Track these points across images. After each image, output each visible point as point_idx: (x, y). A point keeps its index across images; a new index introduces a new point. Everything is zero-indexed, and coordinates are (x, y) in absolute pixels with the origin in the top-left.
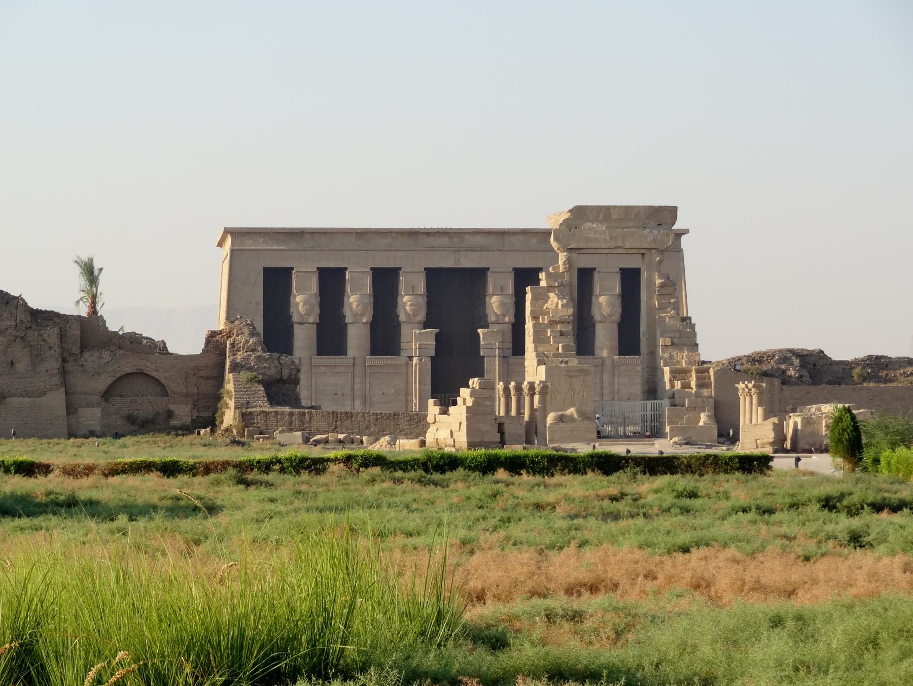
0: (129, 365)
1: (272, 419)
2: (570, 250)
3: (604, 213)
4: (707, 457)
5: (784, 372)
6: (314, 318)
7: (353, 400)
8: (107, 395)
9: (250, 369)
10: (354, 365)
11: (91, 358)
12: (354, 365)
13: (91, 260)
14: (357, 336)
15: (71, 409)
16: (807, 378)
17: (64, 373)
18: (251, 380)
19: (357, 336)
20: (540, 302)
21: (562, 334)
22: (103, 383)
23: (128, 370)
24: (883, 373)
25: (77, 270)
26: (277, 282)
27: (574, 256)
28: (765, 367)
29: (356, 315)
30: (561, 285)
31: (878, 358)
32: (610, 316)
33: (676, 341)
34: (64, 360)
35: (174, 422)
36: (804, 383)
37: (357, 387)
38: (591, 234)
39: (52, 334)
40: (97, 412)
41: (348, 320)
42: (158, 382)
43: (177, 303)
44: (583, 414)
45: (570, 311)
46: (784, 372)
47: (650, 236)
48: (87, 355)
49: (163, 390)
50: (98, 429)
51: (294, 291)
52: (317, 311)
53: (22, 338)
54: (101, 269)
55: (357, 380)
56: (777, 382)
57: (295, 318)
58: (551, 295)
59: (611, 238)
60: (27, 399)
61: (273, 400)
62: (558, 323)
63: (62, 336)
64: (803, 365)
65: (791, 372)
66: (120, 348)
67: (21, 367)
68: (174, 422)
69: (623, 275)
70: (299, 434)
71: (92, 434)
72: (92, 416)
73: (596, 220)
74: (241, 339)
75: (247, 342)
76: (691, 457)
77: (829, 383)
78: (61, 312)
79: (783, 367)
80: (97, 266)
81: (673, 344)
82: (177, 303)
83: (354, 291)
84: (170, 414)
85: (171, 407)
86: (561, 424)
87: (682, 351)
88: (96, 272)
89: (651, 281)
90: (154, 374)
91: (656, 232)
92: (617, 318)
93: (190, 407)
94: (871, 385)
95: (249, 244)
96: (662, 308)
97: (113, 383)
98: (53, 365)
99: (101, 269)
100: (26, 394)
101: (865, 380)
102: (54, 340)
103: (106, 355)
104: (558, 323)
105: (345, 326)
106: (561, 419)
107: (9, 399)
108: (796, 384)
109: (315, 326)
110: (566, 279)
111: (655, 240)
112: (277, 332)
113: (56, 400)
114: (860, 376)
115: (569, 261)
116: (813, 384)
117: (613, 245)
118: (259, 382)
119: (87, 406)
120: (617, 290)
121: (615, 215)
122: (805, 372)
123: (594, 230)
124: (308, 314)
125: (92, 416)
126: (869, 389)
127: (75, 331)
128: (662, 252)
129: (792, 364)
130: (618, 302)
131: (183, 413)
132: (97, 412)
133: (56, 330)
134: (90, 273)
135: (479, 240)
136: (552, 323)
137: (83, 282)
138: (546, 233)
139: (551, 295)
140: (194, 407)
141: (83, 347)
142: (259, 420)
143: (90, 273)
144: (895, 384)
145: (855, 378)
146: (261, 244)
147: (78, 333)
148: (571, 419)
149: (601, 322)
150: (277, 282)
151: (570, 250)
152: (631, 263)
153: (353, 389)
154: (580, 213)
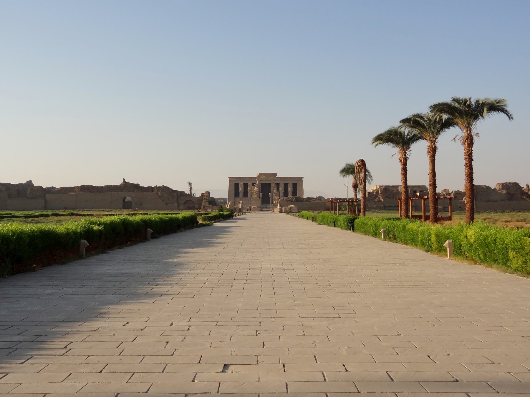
3: (265, 174)
6: (243, 191)
8: (184, 203)
14: (241, 194)
15: (178, 206)
17: (177, 200)
19: (241, 194)
22: (184, 201)
26: (237, 186)
43: (221, 191)
44: (258, 207)
47: (272, 178)
49: (193, 203)
61: (210, 204)
63: (177, 194)
78: (58, 186)
82: (221, 191)
112: (237, 194)
113: (176, 204)
123: (263, 177)
131: (197, 206)
150: (237, 186)
152: (286, 182)
154: (260, 174)
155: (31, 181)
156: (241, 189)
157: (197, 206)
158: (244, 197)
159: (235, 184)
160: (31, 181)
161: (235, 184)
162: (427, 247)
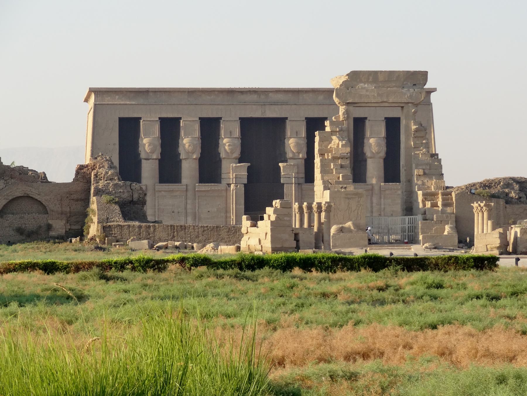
0: (19, 190)
1: (126, 231)
2: (348, 104)
4: (450, 258)
5: (507, 194)
6: (156, 155)
7: (186, 216)
9: (109, 193)
10: (187, 190)
12: (187, 190)
14: (189, 168)
18: (110, 202)
19: (189, 168)
20: (326, 143)
21: (342, 166)
23: (18, 194)
26: (129, 128)
27: (351, 108)
29: (188, 153)
30: (341, 130)
32: (378, 153)
33: (427, 172)
35: (52, 233)
36: (523, 203)
37: (189, 206)
38: (364, 92)
41: (182, 156)
44: (357, 226)
46: (507, 194)
47: (407, 94)
49: (44, 210)
51: (142, 135)
55: (189, 202)
56: (502, 202)
57: (143, 156)
58: (334, 137)
59: (379, 95)
61: (126, 216)
62: (339, 158)
64: (521, 190)
65: (513, 194)
68: (52, 233)
69: (387, 123)
70: (146, 242)
73: (367, 82)
74: (102, 171)
75: (107, 173)
76: (438, 258)
79: (507, 190)
81: (425, 174)
83: (186, 135)
84: (49, 227)
85: (50, 222)
86: (342, 234)
87: (431, 179)
89: (408, 127)
90: (37, 197)
91: (412, 90)
92: (383, 154)
93: (64, 222)
95: (107, 100)
96: (416, 147)
104: (339, 158)
108: (516, 203)
109: (157, 161)
110: (345, 126)
111: (411, 96)
112: (129, 165)
115: (347, 112)
120: (383, 134)
121: (381, 78)
122: (522, 195)
123: (366, 89)
124: (152, 152)
129: (513, 189)
130: (383, 143)
131: (59, 226)
136: (335, 159)
138: (330, 92)
139: (334, 137)
142: (116, 231)
146: (118, 100)
148: (349, 230)
149: (371, 158)
150: (129, 128)
151: (348, 104)
152: (209, 113)
153: (186, 208)
155: (427, 72)
156: (148, 143)
157: (59, 226)
158: (202, 180)
159: (122, 121)
160: (427, 72)
161: (122, 121)
162: (97, 229)
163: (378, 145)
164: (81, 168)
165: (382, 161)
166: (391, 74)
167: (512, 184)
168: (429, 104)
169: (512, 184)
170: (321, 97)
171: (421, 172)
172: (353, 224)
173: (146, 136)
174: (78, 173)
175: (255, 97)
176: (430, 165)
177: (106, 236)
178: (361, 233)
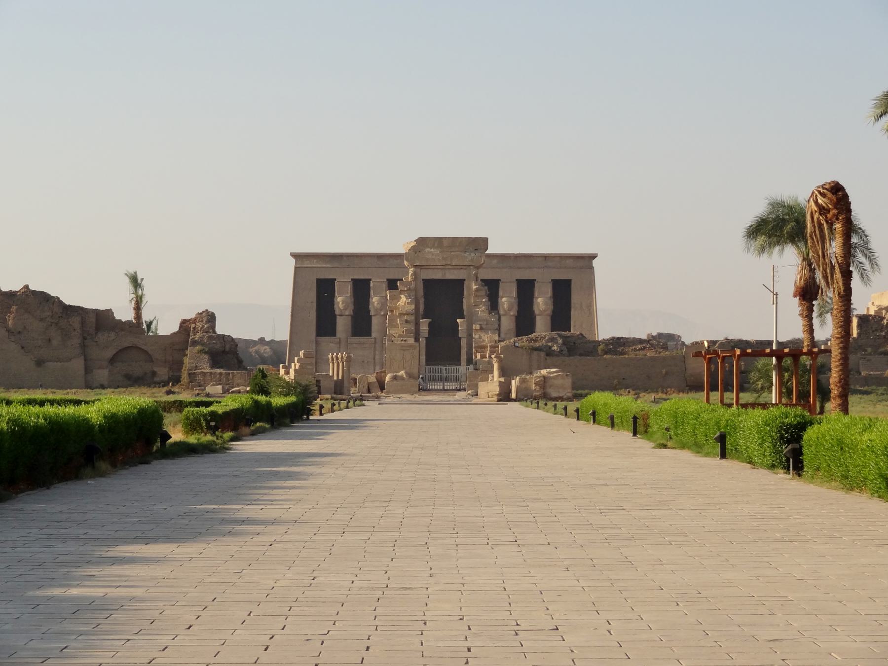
0: (128, 341)
1: (208, 378)
2: (416, 266)
3: (438, 242)
4: (175, 402)
5: (550, 347)
7: (375, 366)
8: (112, 360)
9: (203, 345)
10: (375, 343)
11: (102, 337)
12: (375, 343)
13: (136, 273)
14: (343, 324)
15: (88, 370)
16: (565, 352)
17: (83, 346)
18: (200, 352)
19: (343, 324)
20: (395, 301)
21: (407, 322)
22: (109, 353)
23: (126, 344)
24: (620, 349)
25: (127, 281)
26: (325, 288)
27: (419, 270)
28: (537, 345)
29: (376, 310)
30: (409, 290)
31: (619, 338)
32: (545, 311)
33: (484, 327)
34: (85, 338)
35: (157, 379)
36: (564, 355)
37: (377, 357)
38: (430, 256)
39: (76, 321)
40: (106, 372)
41: (372, 313)
42: (146, 352)
44: (410, 375)
45: (413, 307)
46: (550, 347)
48: (100, 335)
49: (149, 358)
50: (106, 383)
51: (336, 294)
52: (351, 307)
53: (56, 324)
54: (142, 279)
55: (377, 353)
56: (543, 354)
57: (337, 312)
58: (402, 296)
59: (443, 259)
60: (59, 364)
61: (215, 364)
62: (405, 314)
63: (83, 323)
64: (564, 344)
65: (555, 348)
66: (122, 330)
67: (55, 342)
68: (157, 379)
69: (565, 283)
70: (220, 387)
71: (103, 387)
72: (102, 374)
73: (433, 247)
74: (199, 325)
75: (203, 326)
76: (165, 402)
77: (581, 355)
79: (550, 344)
80: (139, 278)
81: (481, 328)
83: (375, 295)
84: (154, 374)
85: (155, 369)
86: (395, 382)
87: (487, 333)
88: (139, 281)
89: (470, 288)
90: (143, 347)
91: (473, 254)
92: (549, 312)
93: (167, 369)
94: (609, 356)
95: (307, 264)
96: (476, 305)
97: (117, 353)
98: (76, 341)
99: (142, 279)
100: (59, 360)
101: (606, 353)
102: (77, 325)
103: (113, 335)
104: (405, 314)
105: (370, 317)
106: (395, 378)
107: (47, 364)
108: (557, 356)
109: (350, 318)
110: (413, 285)
111: (472, 260)
113: (78, 364)
114: (603, 350)
115: (415, 273)
116: (570, 355)
117: (444, 263)
118: (206, 353)
119: (99, 368)
120: (550, 294)
121: (445, 244)
122: (564, 348)
123: (431, 252)
124: (345, 309)
125: (102, 374)
126: (606, 359)
127: (92, 319)
128: (478, 268)
129: (557, 343)
130: (550, 302)
131: (163, 372)
132: (106, 372)
133: (78, 319)
134: (135, 282)
135: (569, 262)
136: (401, 315)
137: (132, 289)
138: (398, 256)
139: (402, 296)
140: (170, 369)
141: (98, 328)
142: (200, 378)
143: (135, 282)
144: (626, 356)
145: (600, 351)
146: (315, 264)
147: (94, 320)
148: (402, 378)
149: (504, 315)
150: (325, 288)
151: (416, 266)
152: (526, 275)
153: (374, 359)
155: (487, 239)
156: (342, 301)
157: (163, 372)
163: (546, 304)
164: (184, 322)
165: (549, 318)
166: (454, 240)
167: (556, 339)
168: (592, 268)
169: (556, 339)
170: (495, 261)
171: (478, 327)
172: (406, 373)
173: (340, 295)
174: (181, 326)
175: (569, 262)
176: (487, 321)
177: (191, 382)
178: (412, 381)
